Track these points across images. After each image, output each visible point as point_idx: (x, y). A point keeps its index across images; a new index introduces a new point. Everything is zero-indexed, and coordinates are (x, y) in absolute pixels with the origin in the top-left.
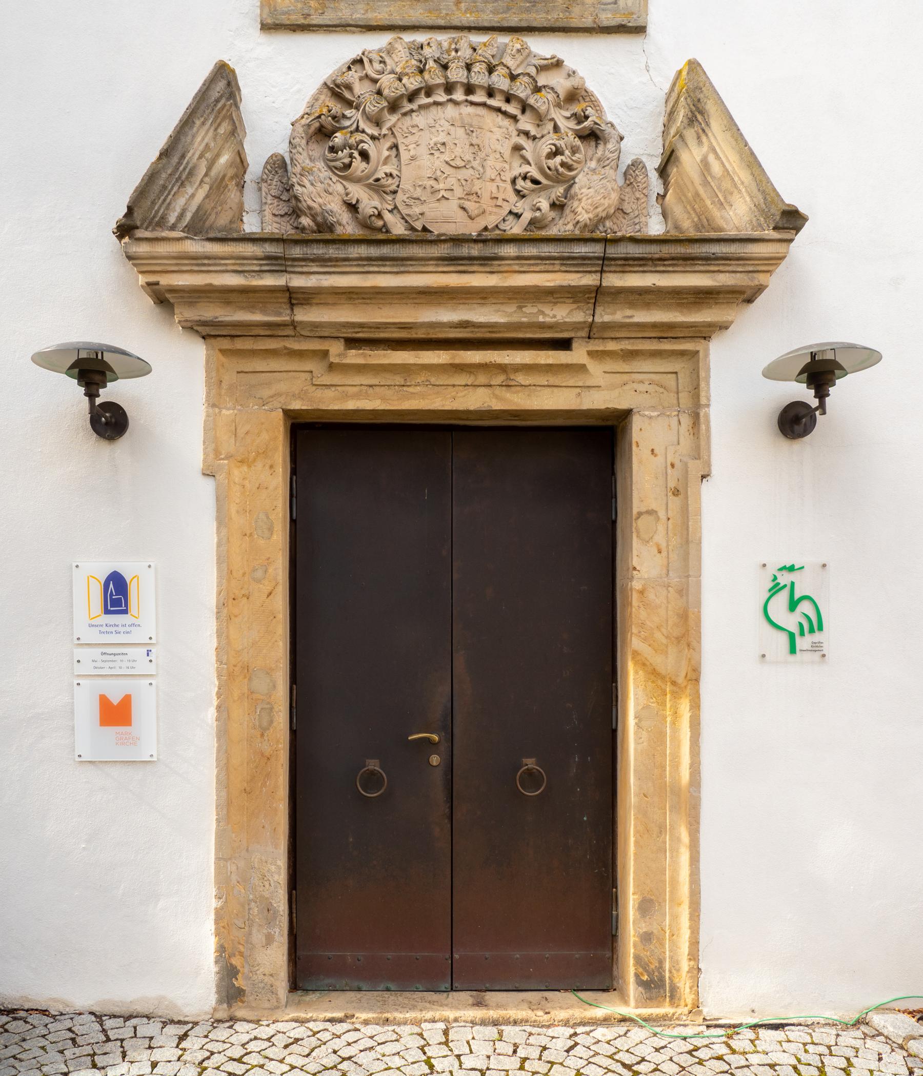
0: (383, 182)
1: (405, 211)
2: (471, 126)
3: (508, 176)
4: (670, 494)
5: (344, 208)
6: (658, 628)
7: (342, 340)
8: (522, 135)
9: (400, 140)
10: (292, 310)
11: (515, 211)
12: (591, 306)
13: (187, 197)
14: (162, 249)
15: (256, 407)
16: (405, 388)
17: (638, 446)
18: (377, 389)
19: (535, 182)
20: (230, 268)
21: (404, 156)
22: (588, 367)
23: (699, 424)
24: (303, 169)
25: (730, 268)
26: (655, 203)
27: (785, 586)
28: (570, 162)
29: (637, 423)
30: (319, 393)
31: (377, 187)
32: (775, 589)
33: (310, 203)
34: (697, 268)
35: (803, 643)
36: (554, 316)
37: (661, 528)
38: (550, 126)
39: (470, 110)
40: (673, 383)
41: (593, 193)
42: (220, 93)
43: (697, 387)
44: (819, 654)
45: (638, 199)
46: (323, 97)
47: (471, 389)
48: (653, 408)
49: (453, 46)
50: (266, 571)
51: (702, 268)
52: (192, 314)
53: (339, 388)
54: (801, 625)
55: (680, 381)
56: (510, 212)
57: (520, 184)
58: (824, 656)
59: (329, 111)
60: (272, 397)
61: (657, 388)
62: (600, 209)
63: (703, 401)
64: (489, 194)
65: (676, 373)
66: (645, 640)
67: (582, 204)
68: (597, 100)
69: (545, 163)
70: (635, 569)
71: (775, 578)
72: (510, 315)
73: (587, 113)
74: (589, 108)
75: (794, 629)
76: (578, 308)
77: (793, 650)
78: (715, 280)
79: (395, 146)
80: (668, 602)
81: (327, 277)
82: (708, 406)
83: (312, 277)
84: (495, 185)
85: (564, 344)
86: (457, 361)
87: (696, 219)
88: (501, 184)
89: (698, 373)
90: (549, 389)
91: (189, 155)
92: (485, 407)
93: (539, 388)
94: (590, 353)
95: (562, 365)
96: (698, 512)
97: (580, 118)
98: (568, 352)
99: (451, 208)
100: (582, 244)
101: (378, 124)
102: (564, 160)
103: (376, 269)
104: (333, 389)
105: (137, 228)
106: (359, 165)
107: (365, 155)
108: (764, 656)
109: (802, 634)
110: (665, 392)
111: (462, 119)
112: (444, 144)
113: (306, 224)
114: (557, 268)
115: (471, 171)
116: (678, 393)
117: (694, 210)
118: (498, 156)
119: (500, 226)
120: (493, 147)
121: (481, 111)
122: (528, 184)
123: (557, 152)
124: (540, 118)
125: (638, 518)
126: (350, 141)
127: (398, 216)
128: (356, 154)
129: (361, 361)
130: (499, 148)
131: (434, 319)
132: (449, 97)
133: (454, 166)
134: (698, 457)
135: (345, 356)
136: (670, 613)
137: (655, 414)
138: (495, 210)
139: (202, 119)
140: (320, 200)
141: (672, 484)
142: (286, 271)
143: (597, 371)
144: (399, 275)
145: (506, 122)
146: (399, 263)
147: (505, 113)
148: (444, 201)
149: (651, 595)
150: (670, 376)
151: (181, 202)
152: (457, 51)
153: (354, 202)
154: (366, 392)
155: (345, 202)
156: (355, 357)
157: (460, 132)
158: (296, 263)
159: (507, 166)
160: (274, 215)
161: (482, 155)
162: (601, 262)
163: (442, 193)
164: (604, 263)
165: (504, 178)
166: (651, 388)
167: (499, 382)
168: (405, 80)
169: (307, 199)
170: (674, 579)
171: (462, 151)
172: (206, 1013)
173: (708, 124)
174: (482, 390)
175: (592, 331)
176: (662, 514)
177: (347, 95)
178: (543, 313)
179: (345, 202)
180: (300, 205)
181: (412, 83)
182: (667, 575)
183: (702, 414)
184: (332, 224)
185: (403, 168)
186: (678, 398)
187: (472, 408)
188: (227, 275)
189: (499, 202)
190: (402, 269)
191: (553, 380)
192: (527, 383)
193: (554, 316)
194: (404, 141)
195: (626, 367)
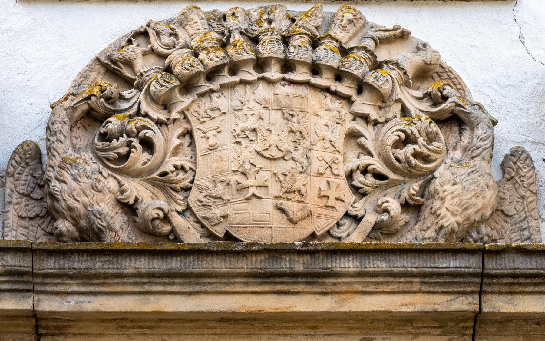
1: (201, 213)
2: (291, 109)
3: (342, 169)
11: (353, 212)
19: (379, 176)
21: (201, 145)
24: (64, 160)
31: (163, 183)
33: (71, 202)
38: (396, 109)
45: (523, 198)
49: (265, 17)
56: (347, 215)
57: (359, 179)
59: (102, 91)
62: (471, 211)
64: (316, 192)
67: (446, 205)
69: (391, 153)
73: (445, 92)
79: (189, 133)
81: (91, 298)
88: (333, 179)
97: (437, 99)
99: (265, 210)
101: (166, 106)
103: (160, 288)
106: (139, 157)
111: (278, 101)
112: (254, 130)
113: (64, 229)
115: (291, 163)
118: (328, 145)
120: (320, 135)
122: (370, 179)
124: (382, 100)
126: (128, 127)
127: (192, 219)
132: (261, 75)
138: (325, 211)
140: (85, 199)
142: (33, 291)
145: (337, 105)
146: (192, 280)
147: (336, 94)
148: (254, 201)
152: (270, 22)
157: (276, 116)
158: (48, 281)
159: (340, 157)
160: (21, 217)
161: (306, 143)
162: (478, 280)
163: (252, 190)
168: (203, 55)
169: (66, 197)
177: (127, 72)
180: (57, 205)
184: (100, 230)
190: (197, 288)
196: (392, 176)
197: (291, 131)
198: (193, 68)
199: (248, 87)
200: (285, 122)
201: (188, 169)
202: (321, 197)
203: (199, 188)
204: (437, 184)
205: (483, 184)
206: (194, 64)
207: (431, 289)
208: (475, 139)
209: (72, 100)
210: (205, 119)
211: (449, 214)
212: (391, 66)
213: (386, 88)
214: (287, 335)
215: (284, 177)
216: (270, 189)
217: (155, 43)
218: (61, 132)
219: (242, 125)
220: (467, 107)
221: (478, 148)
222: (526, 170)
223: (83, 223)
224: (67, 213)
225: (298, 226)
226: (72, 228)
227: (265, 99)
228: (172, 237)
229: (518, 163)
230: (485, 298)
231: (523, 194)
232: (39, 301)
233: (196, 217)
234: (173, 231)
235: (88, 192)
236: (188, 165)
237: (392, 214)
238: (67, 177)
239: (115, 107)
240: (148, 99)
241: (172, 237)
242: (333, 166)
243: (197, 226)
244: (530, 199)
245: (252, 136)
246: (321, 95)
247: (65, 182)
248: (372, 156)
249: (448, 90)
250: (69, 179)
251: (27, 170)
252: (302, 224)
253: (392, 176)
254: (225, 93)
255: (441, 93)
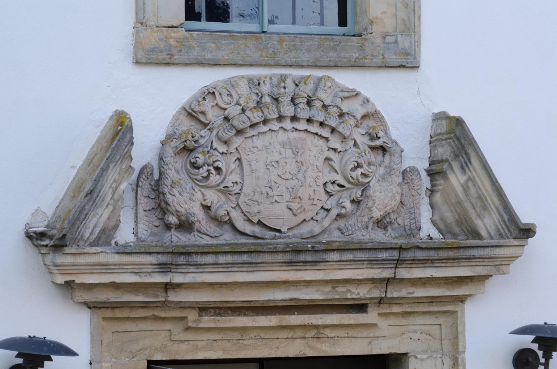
0: (231, 189)
1: (245, 208)
2: (297, 148)
7: (197, 309)
8: (331, 150)
9: (243, 157)
10: (167, 292)
11: (326, 207)
12: (384, 285)
13: (98, 217)
14: (82, 260)
15: (127, 359)
16: (241, 341)
18: (220, 342)
19: (341, 186)
20: (129, 271)
21: (246, 168)
22: (379, 325)
24: (173, 182)
25: (484, 264)
26: (425, 197)
28: (366, 173)
30: (175, 347)
31: (226, 191)
33: (179, 208)
34: (461, 264)
36: (358, 294)
38: (352, 143)
39: (296, 134)
40: (438, 332)
41: (383, 196)
42: (120, 131)
43: (456, 337)
45: (413, 196)
46: (181, 117)
47: (290, 341)
48: (424, 352)
49: (282, 85)
51: (465, 264)
52: (89, 297)
55: (443, 331)
56: (322, 208)
57: (330, 188)
59: (193, 137)
60: (139, 351)
61: (427, 337)
62: (388, 208)
63: (461, 349)
64: (308, 197)
65: (440, 325)
67: (376, 205)
68: (383, 118)
69: (349, 173)
72: (327, 293)
73: (379, 135)
74: (380, 132)
78: (474, 272)
79: (239, 159)
81: (200, 275)
82: (464, 352)
83: (189, 275)
84: (312, 189)
85: (360, 307)
86: (284, 324)
87: (457, 217)
88: (316, 188)
90: (348, 339)
91: (103, 189)
93: (340, 339)
95: (360, 324)
98: (364, 315)
99: (281, 209)
100: (383, 251)
102: (363, 172)
103: (236, 269)
104: (186, 343)
105: (66, 246)
106: (215, 178)
110: (432, 339)
111: (290, 143)
113: (173, 222)
114: (365, 266)
115: (296, 181)
116: (441, 340)
117: (456, 211)
118: (315, 168)
119: (314, 218)
120: (311, 162)
121: (303, 135)
122: (337, 188)
123: (359, 166)
124: (344, 138)
126: (208, 161)
127: (239, 211)
129: (212, 325)
130: (316, 163)
131: (271, 298)
132: (280, 125)
133: (280, 177)
137: (425, 357)
138: (312, 207)
139: (114, 164)
140: (186, 206)
142: (170, 272)
144: (252, 273)
145: (321, 143)
146: (254, 265)
147: (321, 136)
148: (276, 204)
151: (94, 221)
152: (285, 88)
153: (209, 205)
154: (212, 345)
155: (202, 204)
156: (207, 321)
157: (289, 152)
158: (179, 267)
159: (320, 174)
160: (145, 211)
162: (396, 262)
163: (276, 198)
164: (398, 263)
165: (318, 184)
167: (312, 336)
168: (248, 113)
169: (176, 205)
171: (292, 167)
173: (470, 161)
174: (298, 340)
175: (380, 301)
180: (169, 208)
181: (256, 117)
183: (460, 359)
184: (193, 223)
185: (246, 178)
186: (442, 344)
188: (126, 275)
190: (255, 269)
192: (333, 335)
193: (358, 294)
194: (246, 157)
195: (403, 321)
196: (347, 185)
197: (297, 162)
198: (245, 124)
199: (273, 133)
200: (294, 156)
201: (239, 183)
202: (310, 199)
203: (245, 194)
204: (371, 191)
205: (395, 192)
206: (245, 121)
207: (372, 267)
208: (392, 163)
209: (176, 142)
210: (249, 153)
211: (377, 211)
212: (351, 117)
214: (294, 286)
215: (276, 163)
216: (284, 197)
217: (219, 100)
218: (170, 163)
219: (270, 158)
220: (390, 144)
221: (394, 169)
222: (417, 181)
223: (183, 218)
225: (297, 217)
227: (282, 141)
228: (228, 222)
229: (413, 176)
230: (397, 270)
231: (414, 194)
232: (173, 276)
233: (242, 210)
234: (230, 219)
235: (187, 202)
236: (239, 180)
237: (348, 210)
238: (175, 192)
239: (198, 144)
240: (217, 138)
241: (228, 222)
242: (317, 180)
243: (242, 215)
244: (417, 198)
245: (276, 166)
247: (175, 196)
248: (337, 173)
249: (381, 134)
250: (177, 194)
251: (148, 181)
252: (299, 216)
253: (347, 185)
255: (377, 135)
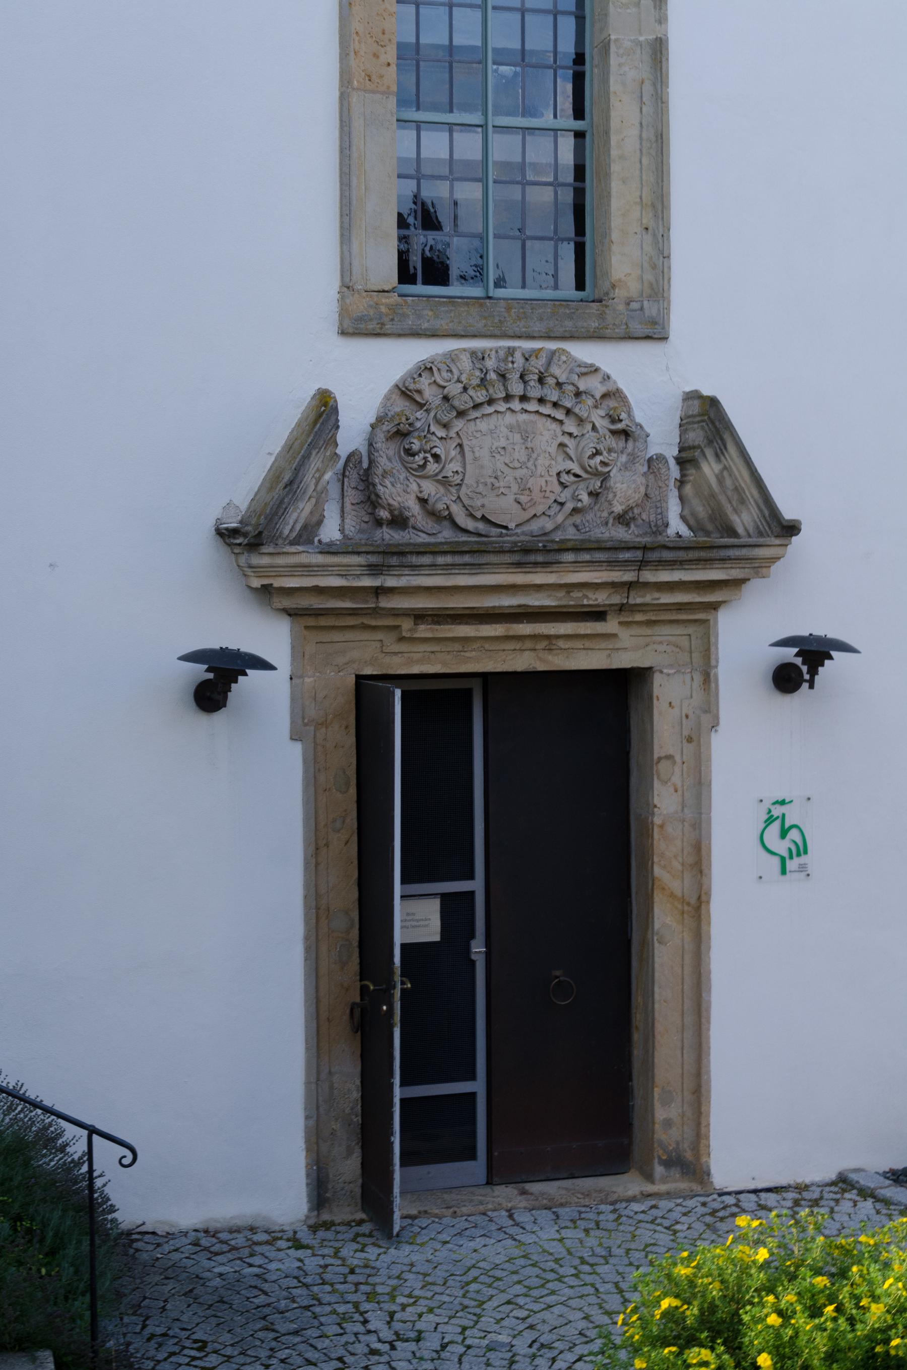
1: (467, 502)
3: (554, 472)
4: (684, 741)
5: (417, 501)
6: (675, 857)
9: (465, 443)
10: (377, 598)
11: (560, 500)
12: (626, 590)
14: (281, 561)
17: (658, 700)
20: (334, 573)
23: (710, 682)
25: (741, 565)
27: (778, 817)
29: (657, 679)
31: (445, 482)
32: (770, 820)
33: (391, 502)
35: (791, 865)
36: (596, 600)
37: (677, 770)
38: (589, 427)
39: (525, 416)
44: (804, 874)
46: (394, 396)
48: (671, 666)
49: (510, 359)
50: (344, 822)
52: (288, 603)
53: (405, 655)
54: (790, 850)
56: (555, 501)
57: (565, 478)
58: (808, 875)
59: (407, 419)
61: (674, 649)
62: (631, 501)
63: (713, 663)
64: (539, 488)
66: (664, 867)
67: (617, 497)
68: (626, 397)
70: (655, 806)
71: (770, 811)
72: (560, 599)
73: (621, 417)
75: (785, 854)
76: (616, 592)
77: (784, 871)
79: (460, 445)
80: (683, 835)
82: (716, 667)
83: (403, 578)
84: (543, 480)
85: (598, 615)
86: (511, 633)
89: (709, 638)
90: (584, 652)
92: (531, 669)
94: (620, 623)
96: (709, 759)
97: (615, 420)
98: (603, 623)
99: (507, 502)
101: (445, 426)
103: (457, 571)
105: (263, 545)
106: (432, 467)
107: (436, 457)
108: (761, 877)
109: (791, 857)
111: (519, 426)
112: (504, 448)
113: (384, 517)
116: (691, 652)
118: (547, 455)
122: (572, 478)
124: (581, 421)
125: (658, 762)
127: (460, 505)
128: (428, 455)
134: (707, 711)
135: (415, 630)
136: (685, 844)
138: (543, 500)
140: (399, 499)
141: (686, 733)
143: (626, 637)
147: (554, 419)
148: (502, 496)
149: (669, 829)
150: (684, 637)
151: (294, 516)
152: (513, 362)
155: (418, 497)
156: (424, 630)
159: (553, 462)
160: (353, 504)
161: (534, 456)
163: (502, 490)
164: (642, 564)
166: (669, 649)
168: (471, 392)
169: (388, 497)
170: (689, 814)
171: (520, 454)
172: (299, 1221)
173: (726, 448)
174: (527, 653)
175: (621, 608)
176: (678, 758)
177: (417, 397)
178: (586, 597)
179: (418, 497)
180: (380, 501)
182: (683, 810)
183: (712, 675)
187: (519, 670)
189: (547, 494)
191: (588, 644)
192: (567, 646)
193: (596, 600)
195: (648, 631)
196: (584, 475)
213: (584, 414)
219: (496, 444)
223: (396, 513)
224: (387, 507)
226: (389, 516)
230: (641, 572)
238: (387, 483)
243: (464, 509)
246: (544, 419)
250: (389, 485)
252: (530, 510)
253: (584, 475)
254: (485, 419)
